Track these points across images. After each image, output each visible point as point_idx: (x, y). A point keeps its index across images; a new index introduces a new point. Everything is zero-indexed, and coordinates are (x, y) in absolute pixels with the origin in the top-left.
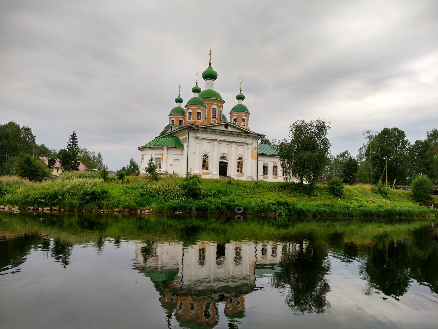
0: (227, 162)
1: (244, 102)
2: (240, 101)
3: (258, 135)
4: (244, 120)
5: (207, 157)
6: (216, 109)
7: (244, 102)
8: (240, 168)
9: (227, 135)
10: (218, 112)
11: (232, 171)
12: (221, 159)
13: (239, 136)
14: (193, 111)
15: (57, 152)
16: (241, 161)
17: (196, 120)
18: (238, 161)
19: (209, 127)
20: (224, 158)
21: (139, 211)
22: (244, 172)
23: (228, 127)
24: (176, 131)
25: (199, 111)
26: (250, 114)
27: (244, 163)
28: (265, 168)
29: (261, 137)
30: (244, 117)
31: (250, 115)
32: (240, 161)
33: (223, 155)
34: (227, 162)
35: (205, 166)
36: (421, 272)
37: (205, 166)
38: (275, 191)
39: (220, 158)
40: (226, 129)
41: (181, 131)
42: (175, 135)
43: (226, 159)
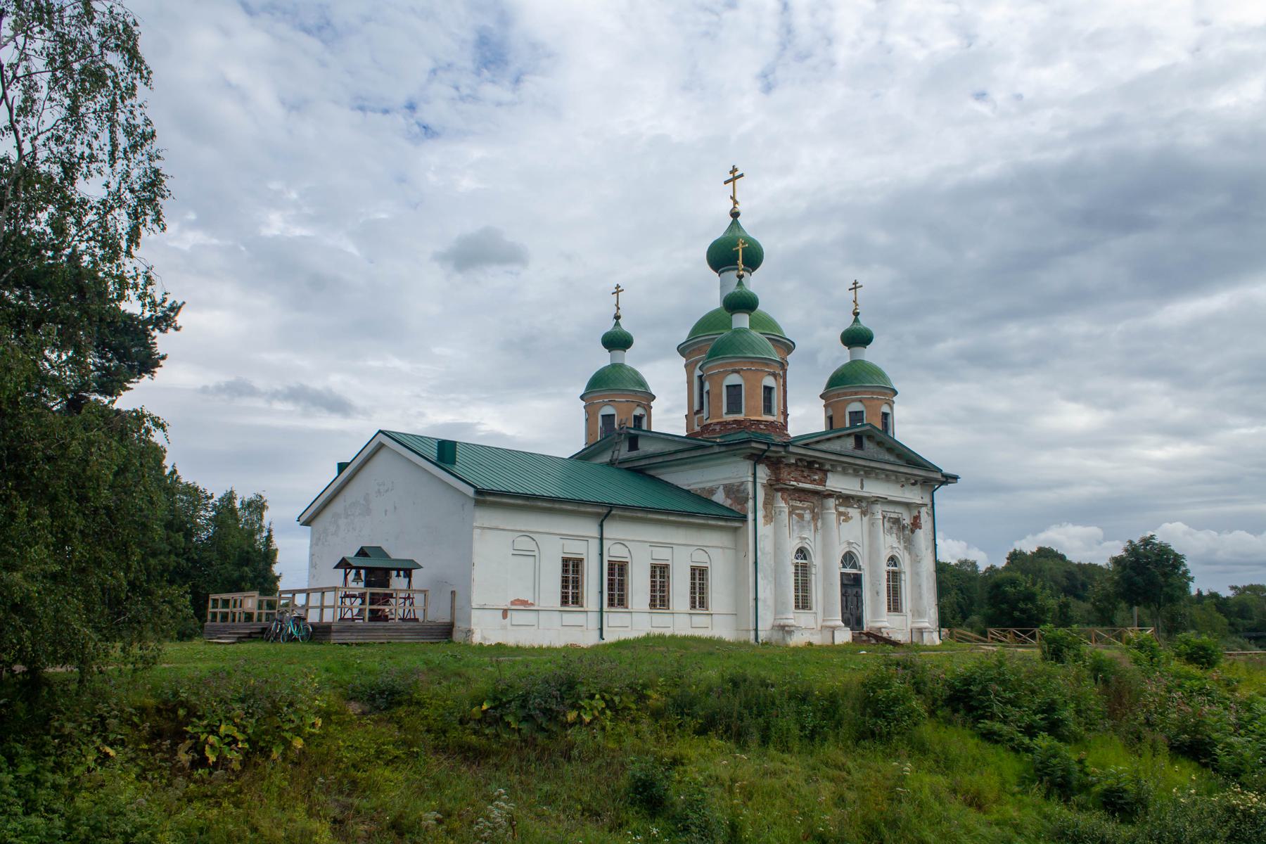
0: (861, 575)
1: (869, 354)
2: (618, 353)
3: (943, 475)
4: (885, 415)
7: (869, 354)
8: (895, 605)
10: (722, 401)
12: (844, 567)
14: (617, 411)
17: (761, 416)
19: (818, 442)
23: (866, 443)
26: (895, 393)
28: (572, 569)
29: (949, 480)
30: (885, 409)
31: (895, 399)
33: (800, 545)
34: (861, 575)
35: (803, 602)
37: (803, 602)
39: (842, 562)
40: (634, 453)
41: (723, 454)
42: (652, 473)
43: (854, 566)
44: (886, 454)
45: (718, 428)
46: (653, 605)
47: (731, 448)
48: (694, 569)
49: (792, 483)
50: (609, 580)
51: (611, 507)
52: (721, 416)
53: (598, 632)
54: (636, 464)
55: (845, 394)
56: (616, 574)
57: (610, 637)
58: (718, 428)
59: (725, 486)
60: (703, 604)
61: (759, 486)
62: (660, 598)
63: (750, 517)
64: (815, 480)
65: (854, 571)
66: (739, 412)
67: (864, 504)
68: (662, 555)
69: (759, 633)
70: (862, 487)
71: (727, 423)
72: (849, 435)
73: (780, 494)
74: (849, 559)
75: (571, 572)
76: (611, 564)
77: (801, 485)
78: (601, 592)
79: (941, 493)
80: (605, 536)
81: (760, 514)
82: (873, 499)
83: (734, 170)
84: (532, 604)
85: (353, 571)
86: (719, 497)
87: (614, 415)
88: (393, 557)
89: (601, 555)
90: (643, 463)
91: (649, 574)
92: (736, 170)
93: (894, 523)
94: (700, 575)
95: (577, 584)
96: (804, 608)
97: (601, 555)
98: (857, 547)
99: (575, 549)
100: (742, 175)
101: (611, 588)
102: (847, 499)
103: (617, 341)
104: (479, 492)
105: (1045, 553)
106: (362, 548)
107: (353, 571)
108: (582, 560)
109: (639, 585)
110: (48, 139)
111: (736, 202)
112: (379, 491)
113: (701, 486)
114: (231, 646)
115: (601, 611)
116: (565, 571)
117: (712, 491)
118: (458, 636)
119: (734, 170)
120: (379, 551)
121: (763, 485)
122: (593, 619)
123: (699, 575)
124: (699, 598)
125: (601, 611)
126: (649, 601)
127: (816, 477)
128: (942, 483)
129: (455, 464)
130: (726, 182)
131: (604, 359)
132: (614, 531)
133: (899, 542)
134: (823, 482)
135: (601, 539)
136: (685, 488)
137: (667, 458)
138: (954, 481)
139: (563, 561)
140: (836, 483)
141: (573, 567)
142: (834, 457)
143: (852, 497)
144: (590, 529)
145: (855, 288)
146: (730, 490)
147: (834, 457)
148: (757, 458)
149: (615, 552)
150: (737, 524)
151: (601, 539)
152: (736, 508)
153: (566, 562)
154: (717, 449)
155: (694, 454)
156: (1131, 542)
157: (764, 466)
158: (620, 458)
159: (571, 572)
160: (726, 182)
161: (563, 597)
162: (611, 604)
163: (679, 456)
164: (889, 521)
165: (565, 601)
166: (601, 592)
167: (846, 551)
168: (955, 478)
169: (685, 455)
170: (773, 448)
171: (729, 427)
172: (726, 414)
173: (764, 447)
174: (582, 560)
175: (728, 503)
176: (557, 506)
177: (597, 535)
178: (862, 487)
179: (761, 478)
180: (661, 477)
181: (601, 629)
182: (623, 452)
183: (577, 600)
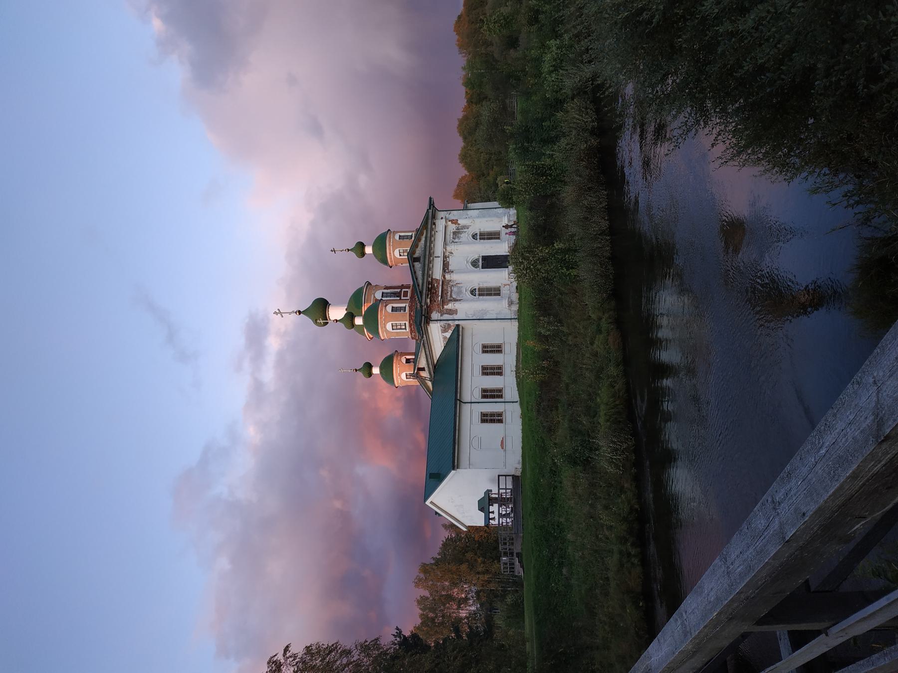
0: (482, 256)
5: (475, 289)
6: (383, 293)
8: (492, 236)
9: (431, 265)
10: (458, 527)
11: (501, 248)
13: (433, 239)
15: (466, 172)
16: (478, 235)
18: (477, 296)
19: (424, 344)
21: (772, 39)
22: (500, 285)
23: (416, 255)
24: (428, 353)
25: (389, 308)
27: (481, 286)
29: (432, 203)
32: (477, 293)
33: (469, 292)
35: (494, 292)
36: (544, 317)
38: (468, 583)
39: (476, 268)
42: (435, 362)
44: (421, 242)
45: (413, 334)
46: (500, 374)
47: (424, 333)
49: (439, 300)
50: (490, 398)
51: (456, 399)
52: (408, 332)
54: (432, 370)
55: (391, 258)
56: (488, 394)
57: (517, 398)
58: (413, 334)
59: (442, 332)
60: (499, 346)
61: (442, 318)
62: (496, 371)
63: (457, 323)
64: (437, 286)
65: (481, 260)
66: (407, 297)
67: (447, 254)
68: (478, 370)
69: (512, 318)
70: (439, 257)
71: (411, 330)
72: (413, 266)
73: (445, 306)
74: (474, 264)
75: (487, 418)
76: (484, 397)
77: (440, 294)
78: (496, 402)
80: (469, 401)
81: (455, 317)
82: (444, 250)
83: (275, 313)
84: (503, 438)
85: (491, 521)
86: (448, 335)
88: (483, 496)
89: (478, 403)
90: (431, 367)
91: (487, 354)
93: (456, 235)
95: (492, 415)
96: (499, 235)
97: (478, 403)
98: (469, 259)
99: (477, 418)
100: (279, 310)
102: (446, 266)
104: (454, 469)
106: (479, 510)
107: (491, 521)
108: (481, 413)
109: (492, 382)
110: (470, 606)
112: (452, 502)
113: (442, 342)
114: (525, 570)
115: (505, 402)
116: (484, 239)
117: (445, 338)
118: (518, 473)
119: (332, 251)
120: (480, 502)
121: (441, 315)
123: (488, 349)
124: (496, 349)
125: (505, 402)
126: (499, 376)
127: (436, 285)
128: (434, 207)
132: (467, 397)
133: (465, 232)
134: (437, 281)
135: (471, 403)
136: (443, 348)
137: (429, 357)
138: (432, 200)
140: (437, 273)
142: (426, 277)
143: (444, 261)
144: (466, 409)
146: (445, 330)
147: (426, 277)
148: (428, 320)
149: (477, 396)
150: (461, 329)
151: (471, 403)
152: (453, 328)
153: (483, 421)
154: (425, 338)
155: (427, 347)
156: (458, 119)
157: (432, 315)
158: (429, 377)
159: (487, 418)
161: (499, 422)
162: (501, 397)
163: (428, 353)
164: (455, 239)
165: (500, 421)
166: (496, 402)
167: (470, 265)
169: (427, 350)
170: (423, 313)
171: (413, 329)
173: (423, 317)
174: (481, 413)
175: (450, 332)
176: (457, 428)
177: (470, 404)
178: (439, 257)
179: (438, 316)
180: (438, 357)
181: (513, 402)
183: (500, 415)
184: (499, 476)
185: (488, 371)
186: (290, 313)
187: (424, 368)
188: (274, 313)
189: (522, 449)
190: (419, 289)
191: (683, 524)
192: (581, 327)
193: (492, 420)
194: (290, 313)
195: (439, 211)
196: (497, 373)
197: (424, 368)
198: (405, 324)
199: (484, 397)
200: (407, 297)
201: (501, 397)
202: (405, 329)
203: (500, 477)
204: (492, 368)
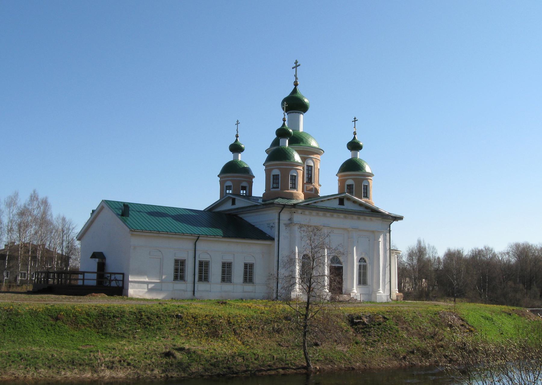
1: (360, 155)
7: (360, 155)
19: (315, 202)
20: (336, 261)
23: (346, 202)
40: (341, 207)
46: (176, 278)
48: (246, 264)
53: (192, 293)
54: (234, 214)
61: (281, 225)
63: (276, 239)
68: (228, 259)
76: (201, 263)
78: (194, 275)
79: (394, 225)
83: (238, 121)
87: (231, 186)
90: (236, 213)
92: (356, 118)
94: (249, 267)
95: (183, 271)
100: (357, 120)
101: (200, 271)
103: (236, 148)
105: (380, 238)
108: (185, 260)
111: (296, 78)
119: (355, 118)
122: (190, 287)
123: (249, 270)
129: (128, 217)
130: (293, 68)
131: (229, 157)
139: (245, 264)
141: (181, 263)
145: (355, 121)
149: (202, 256)
160: (293, 68)
162: (200, 279)
166: (194, 275)
168: (401, 218)
172: (272, 188)
174: (185, 260)
181: (194, 291)
182: (228, 206)
184: (123, 274)
185: (227, 268)
186: (296, 76)
187: (235, 205)
188: (296, 60)
189: (112, 295)
190: (311, 203)
191: (470, 378)
192: (92, 356)
193: (177, 270)
194: (296, 76)
195: (280, 213)
196: (246, 277)
197: (235, 205)
198: (278, 188)
199: (201, 263)
200: (312, 191)
201: (200, 279)
202: (273, 188)
203: (122, 276)
204: (251, 273)
